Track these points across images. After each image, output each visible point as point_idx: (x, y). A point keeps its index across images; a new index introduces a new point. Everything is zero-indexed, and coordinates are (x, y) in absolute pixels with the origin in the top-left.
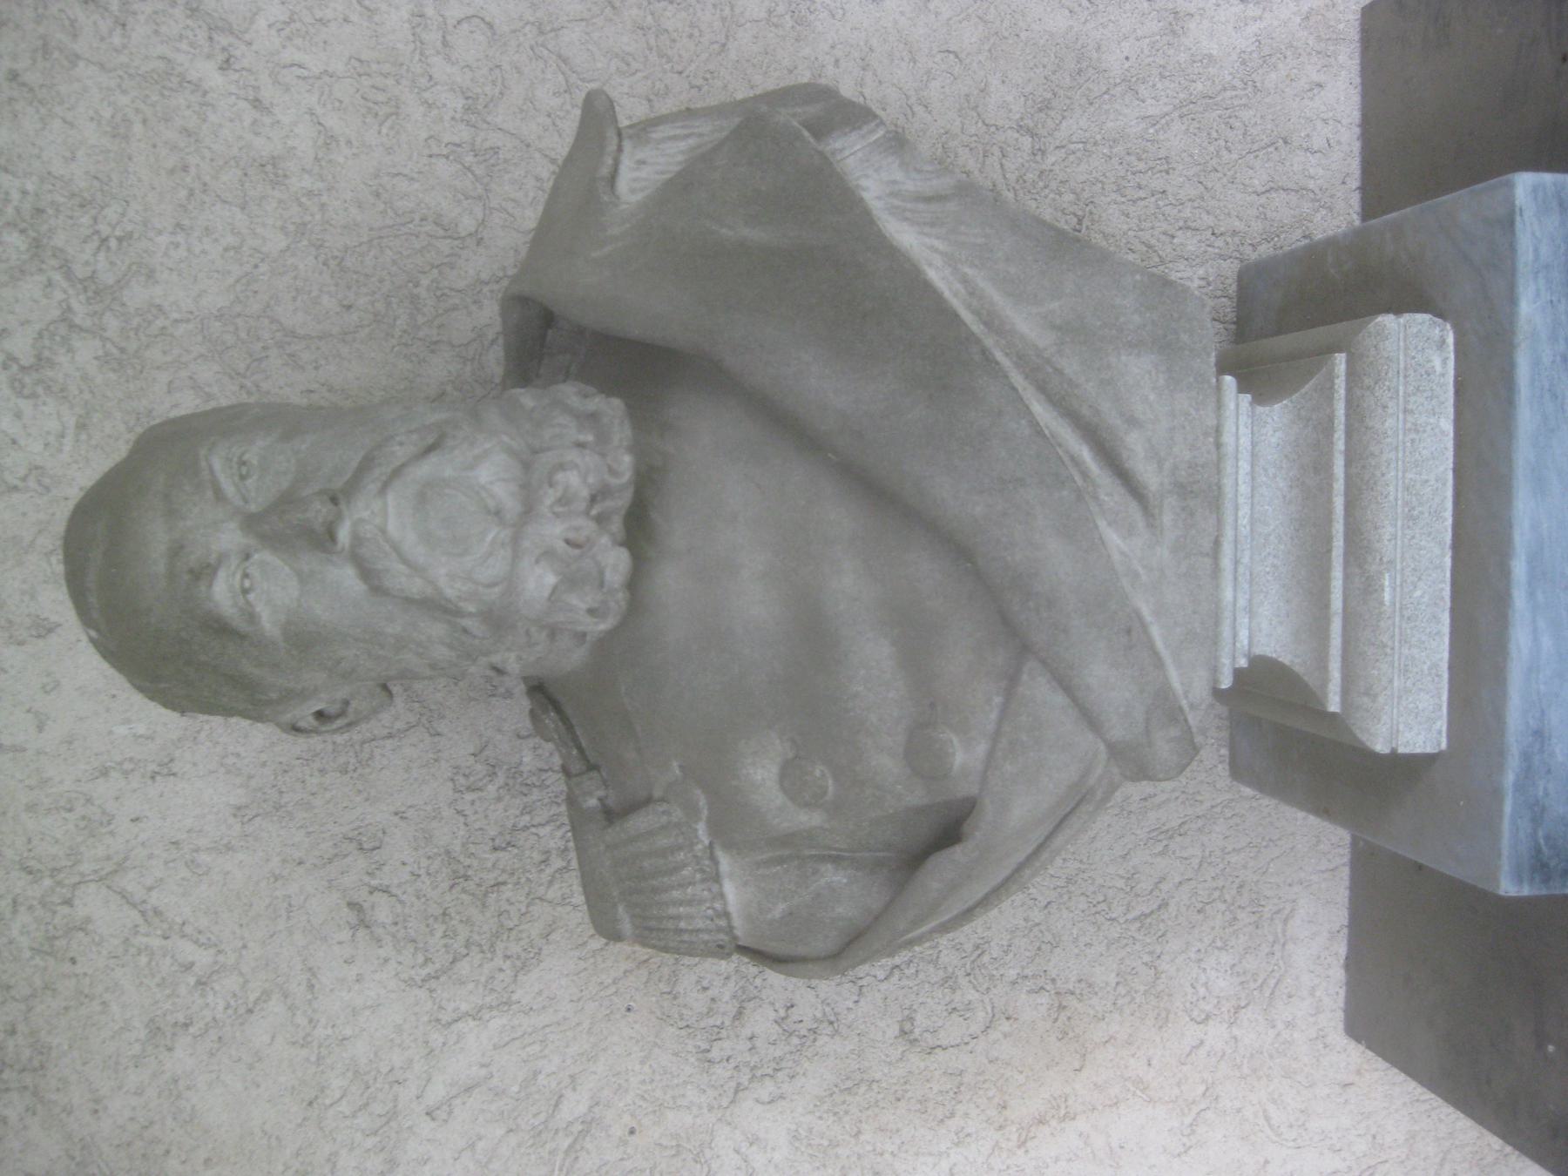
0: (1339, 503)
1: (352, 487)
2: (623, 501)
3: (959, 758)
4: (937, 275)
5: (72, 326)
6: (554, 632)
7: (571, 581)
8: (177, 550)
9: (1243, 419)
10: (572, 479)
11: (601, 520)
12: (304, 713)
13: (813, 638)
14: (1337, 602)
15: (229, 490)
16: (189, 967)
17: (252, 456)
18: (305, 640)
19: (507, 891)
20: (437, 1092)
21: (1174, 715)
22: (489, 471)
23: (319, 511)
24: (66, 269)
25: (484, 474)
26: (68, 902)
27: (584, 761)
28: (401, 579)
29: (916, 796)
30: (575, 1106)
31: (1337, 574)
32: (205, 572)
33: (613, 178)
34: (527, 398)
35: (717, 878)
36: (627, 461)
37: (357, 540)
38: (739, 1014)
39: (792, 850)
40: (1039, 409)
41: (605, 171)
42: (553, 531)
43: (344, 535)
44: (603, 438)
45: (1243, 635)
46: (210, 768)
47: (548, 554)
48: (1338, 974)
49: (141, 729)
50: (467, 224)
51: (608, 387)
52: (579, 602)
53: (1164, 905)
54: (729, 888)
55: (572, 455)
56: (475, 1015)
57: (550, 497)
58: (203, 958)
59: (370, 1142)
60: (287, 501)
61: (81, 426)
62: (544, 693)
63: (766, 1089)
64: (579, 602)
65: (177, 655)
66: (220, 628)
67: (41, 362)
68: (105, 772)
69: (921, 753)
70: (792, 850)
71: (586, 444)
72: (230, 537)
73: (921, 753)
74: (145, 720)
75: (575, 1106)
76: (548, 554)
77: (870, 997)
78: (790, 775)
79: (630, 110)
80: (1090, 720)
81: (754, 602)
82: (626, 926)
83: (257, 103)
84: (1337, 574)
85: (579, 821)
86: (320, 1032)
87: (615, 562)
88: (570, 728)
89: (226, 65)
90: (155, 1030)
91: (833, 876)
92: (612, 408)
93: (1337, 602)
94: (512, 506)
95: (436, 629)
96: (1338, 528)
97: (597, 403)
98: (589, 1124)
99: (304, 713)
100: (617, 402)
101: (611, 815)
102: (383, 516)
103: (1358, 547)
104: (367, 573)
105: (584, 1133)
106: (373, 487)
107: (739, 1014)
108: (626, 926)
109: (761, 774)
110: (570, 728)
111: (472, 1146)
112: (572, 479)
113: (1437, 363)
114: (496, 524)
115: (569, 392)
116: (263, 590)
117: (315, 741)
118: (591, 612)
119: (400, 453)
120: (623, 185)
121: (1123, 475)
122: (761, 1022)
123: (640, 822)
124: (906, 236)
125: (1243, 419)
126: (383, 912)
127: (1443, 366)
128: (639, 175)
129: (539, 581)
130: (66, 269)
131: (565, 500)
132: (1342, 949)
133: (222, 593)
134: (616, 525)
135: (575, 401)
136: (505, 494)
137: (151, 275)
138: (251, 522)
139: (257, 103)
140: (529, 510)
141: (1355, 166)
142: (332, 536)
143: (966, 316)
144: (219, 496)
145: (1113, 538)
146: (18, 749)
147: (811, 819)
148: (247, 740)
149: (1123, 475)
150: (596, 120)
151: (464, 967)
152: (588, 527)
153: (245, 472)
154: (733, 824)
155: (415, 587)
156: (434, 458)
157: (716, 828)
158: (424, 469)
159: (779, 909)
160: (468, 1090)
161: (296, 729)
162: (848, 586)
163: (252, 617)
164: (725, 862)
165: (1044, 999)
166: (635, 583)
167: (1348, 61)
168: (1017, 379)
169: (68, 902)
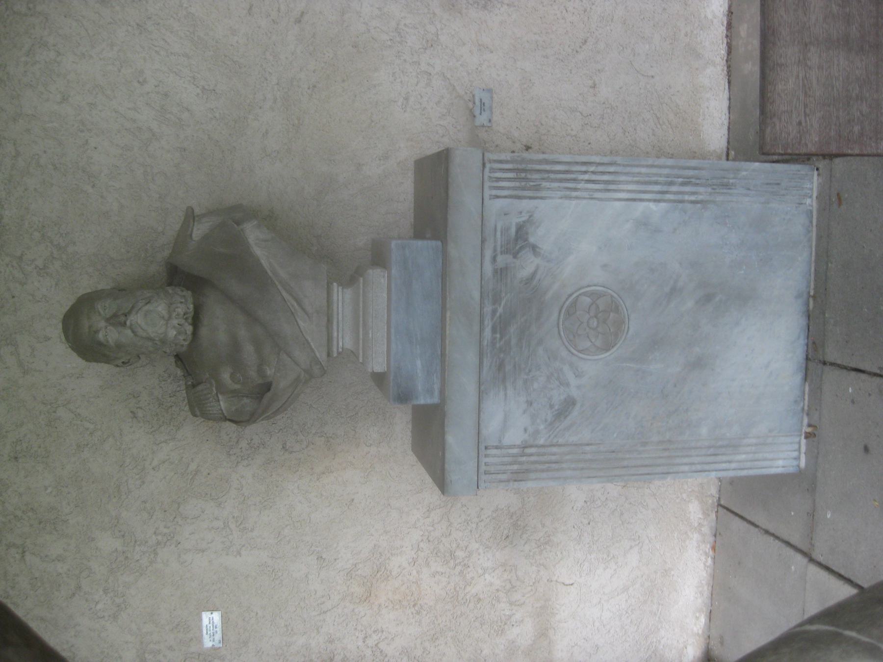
0: (361, 313)
1: (130, 312)
2: (191, 315)
3: (269, 372)
4: (264, 262)
5: (53, 258)
6: (176, 345)
7: (179, 333)
8: (90, 327)
9: (340, 293)
10: (179, 310)
11: (186, 319)
12: (119, 362)
13: (235, 346)
14: (361, 337)
15: (102, 312)
16: (87, 429)
17: (107, 305)
18: (119, 346)
19: (174, 408)
20: (155, 463)
21: (318, 362)
22: (161, 307)
23: (122, 319)
24: (51, 242)
25: (160, 309)
26: (55, 412)
27: (188, 373)
28: (140, 332)
29: (260, 381)
30: (193, 467)
31: (361, 330)
32: (97, 332)
33: (191, 235)
34: (170, 290)
35: (219, 401)
36: (191, 306)
37: (131, 325)
38: (237, 442)
39: (235, 394)
40: (284, 294)
41: (189, 233)
42: (175, 322)
43: (128, 323)
44: (186, 301)
45: (341, 344)
46: (96, 374)
47: (174, 327)
48: (409, 434)
49: (74, 365)
50: (160, 229)
51: (188, 289)
52: (181, 338)
53: (357, 413)
54: (221, 403)
55: (179, 305)
56: (165, 442)
57: (174, 315)
58: (92, 427)
59: (137, 477)
60: (115, 315)
61: (57, 284)
62: (178, 357)
63: (245, 463)
64: (181, 338)
65: (89, 349)
66: (100, 344)
67: (45, 267)
68: (64, 377)
69: (261, 372)
70: (235, 394)
71: (183, 303)
72: (103, 324)
73: (261, 372)
74: (76, 362)
75: (193, 467)
76: (174, 327)
77: (254, 430)
78: (232, 377)
79: (197, 211)
80: (297, 363)
81: (222, 337)
82: (198, 413)
83: (102, 197)
84: (361, 330)
85: (187, 387)
86: (123, 447)
87: (189, 329)
88: (184, 365)
89: (93, 186)
90: (78, 446)
91: (246, 401)
92: (188, 294)
93: (361, 337)
94: (166, 316)
95: (150, 344)
96: (361, 319)
97: (185, 293)
98: (197, 472)
99: (119, 362)
100: (190, 293)
101: (194, 386)
102: (137, 319)
103: (365, 324)
104: (133, 332)
105: (196, 474)
106: (134, 313)
107: (237, 442)
108: (198, 413)
109: (226, 376)
110: (184, 365)
111: (165, 478)
112: (179, 310)
113: (382, 281)
114: (161, 319)
115: (178, 290)
116: (110, 335)
117: (122, 369)
118: (184, 340)
119: (140, 304)
120: (194, 236)
121: (303, 309)
122: (244, 444)
123: (200, 387)
124: (258, 252)
125: (340, 293)
126: (140, 414)
127: (384, 281)
128: (199, 231)
129: (172, 333)
130: (51, 242)
131: (178, 315)
132: (410, 426)
133: (101, 336)
134: (190, 320)
135: (180, 293)
136: (165, 313)
137: (74, 243)
138: (108, 320)
139: (102, 197)
140: (170, 318)
141: (412, 205)
142: (125, 323)
143: (269, 271)
144: (100, 314)
145: (301, 323)
146: (40, 371)
147: (237, 387)
148: (104, 369)
149: (303, 309)
150: (191, 216)
151: (163, 428)
152: (183, 321)
153: (106, 308)
154: (221, 388)
155: (144, 335)
156: (148, 305)
157: (217, 389)
158: (147, 308)
159: (233, 408)
160: (164, 462)
161: (118, 366)
162: (243, 333)
163: (108, 342)
164: (220, 397)
165: (323, 439)
166: (195, 333)
167: (411, 175)
168: (280, 287)
169: (55, 412)
